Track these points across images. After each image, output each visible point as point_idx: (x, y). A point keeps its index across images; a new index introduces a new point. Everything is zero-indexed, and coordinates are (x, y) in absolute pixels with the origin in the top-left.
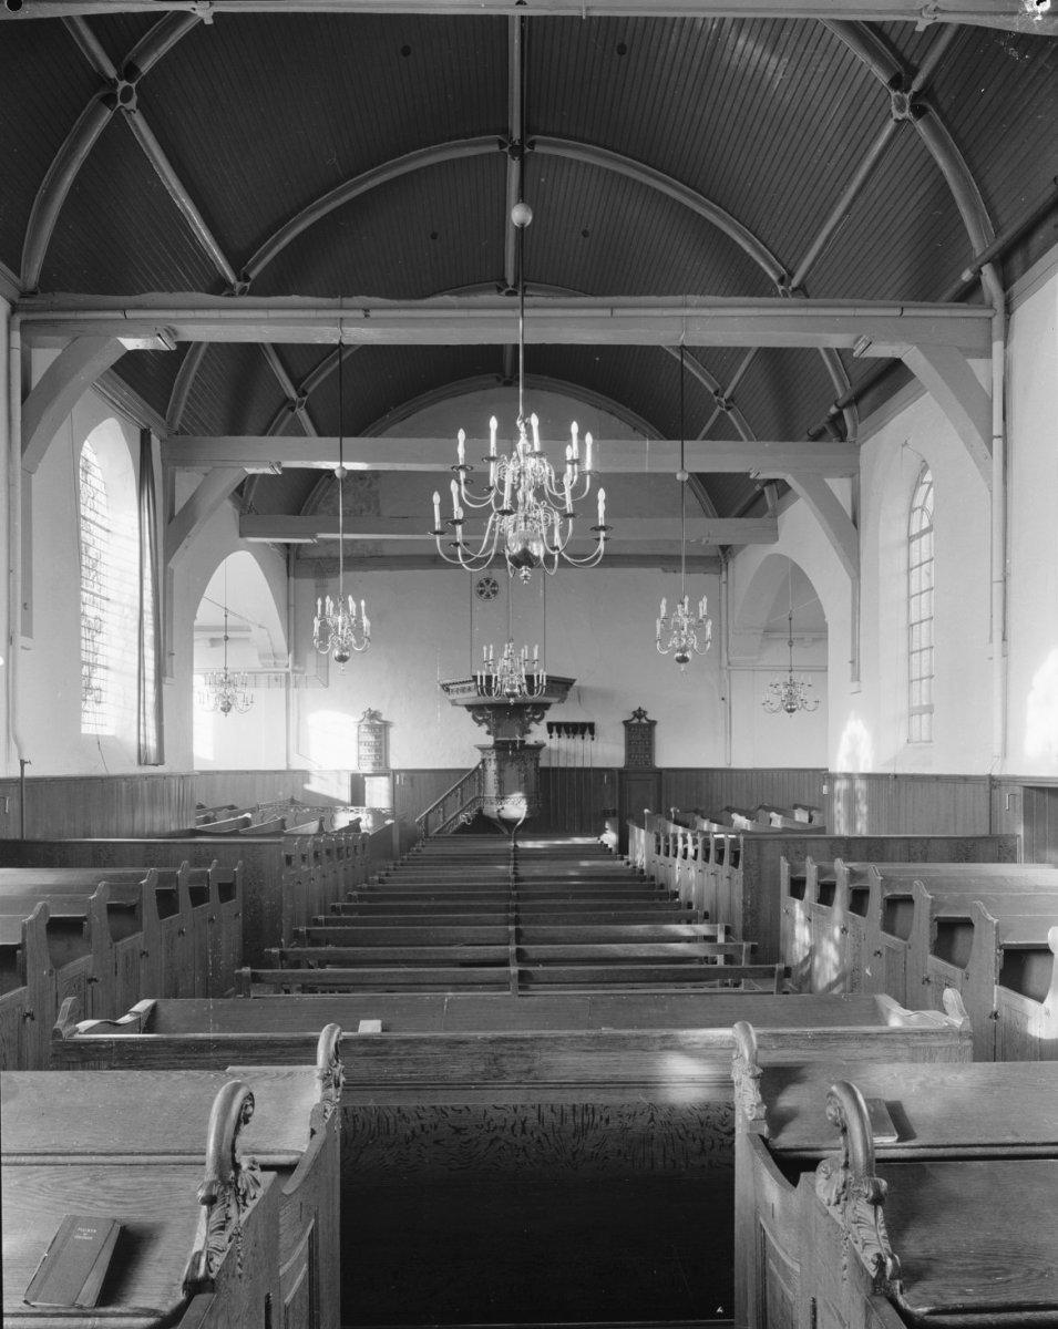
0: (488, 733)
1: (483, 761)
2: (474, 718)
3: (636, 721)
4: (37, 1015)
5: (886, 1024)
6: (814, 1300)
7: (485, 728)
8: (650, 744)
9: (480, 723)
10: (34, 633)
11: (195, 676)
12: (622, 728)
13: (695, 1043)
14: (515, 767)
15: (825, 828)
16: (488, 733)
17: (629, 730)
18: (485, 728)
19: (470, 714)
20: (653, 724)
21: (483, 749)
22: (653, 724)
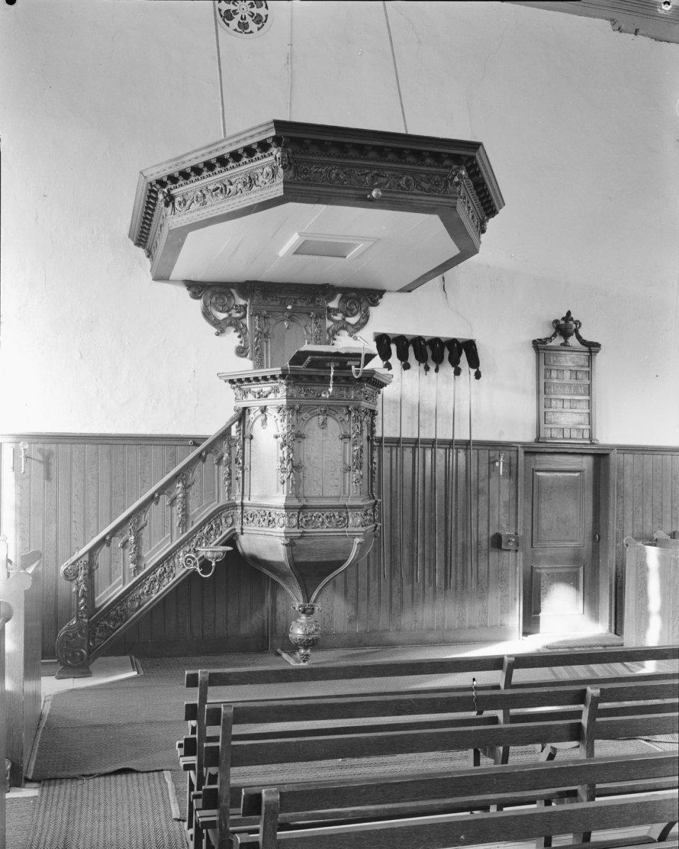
0: (241, 352)
1: (242, 416)
2: (207, 314)
7: (232, 339)
9: (220, 327)
16: (241, 352)
18: (232, 339)
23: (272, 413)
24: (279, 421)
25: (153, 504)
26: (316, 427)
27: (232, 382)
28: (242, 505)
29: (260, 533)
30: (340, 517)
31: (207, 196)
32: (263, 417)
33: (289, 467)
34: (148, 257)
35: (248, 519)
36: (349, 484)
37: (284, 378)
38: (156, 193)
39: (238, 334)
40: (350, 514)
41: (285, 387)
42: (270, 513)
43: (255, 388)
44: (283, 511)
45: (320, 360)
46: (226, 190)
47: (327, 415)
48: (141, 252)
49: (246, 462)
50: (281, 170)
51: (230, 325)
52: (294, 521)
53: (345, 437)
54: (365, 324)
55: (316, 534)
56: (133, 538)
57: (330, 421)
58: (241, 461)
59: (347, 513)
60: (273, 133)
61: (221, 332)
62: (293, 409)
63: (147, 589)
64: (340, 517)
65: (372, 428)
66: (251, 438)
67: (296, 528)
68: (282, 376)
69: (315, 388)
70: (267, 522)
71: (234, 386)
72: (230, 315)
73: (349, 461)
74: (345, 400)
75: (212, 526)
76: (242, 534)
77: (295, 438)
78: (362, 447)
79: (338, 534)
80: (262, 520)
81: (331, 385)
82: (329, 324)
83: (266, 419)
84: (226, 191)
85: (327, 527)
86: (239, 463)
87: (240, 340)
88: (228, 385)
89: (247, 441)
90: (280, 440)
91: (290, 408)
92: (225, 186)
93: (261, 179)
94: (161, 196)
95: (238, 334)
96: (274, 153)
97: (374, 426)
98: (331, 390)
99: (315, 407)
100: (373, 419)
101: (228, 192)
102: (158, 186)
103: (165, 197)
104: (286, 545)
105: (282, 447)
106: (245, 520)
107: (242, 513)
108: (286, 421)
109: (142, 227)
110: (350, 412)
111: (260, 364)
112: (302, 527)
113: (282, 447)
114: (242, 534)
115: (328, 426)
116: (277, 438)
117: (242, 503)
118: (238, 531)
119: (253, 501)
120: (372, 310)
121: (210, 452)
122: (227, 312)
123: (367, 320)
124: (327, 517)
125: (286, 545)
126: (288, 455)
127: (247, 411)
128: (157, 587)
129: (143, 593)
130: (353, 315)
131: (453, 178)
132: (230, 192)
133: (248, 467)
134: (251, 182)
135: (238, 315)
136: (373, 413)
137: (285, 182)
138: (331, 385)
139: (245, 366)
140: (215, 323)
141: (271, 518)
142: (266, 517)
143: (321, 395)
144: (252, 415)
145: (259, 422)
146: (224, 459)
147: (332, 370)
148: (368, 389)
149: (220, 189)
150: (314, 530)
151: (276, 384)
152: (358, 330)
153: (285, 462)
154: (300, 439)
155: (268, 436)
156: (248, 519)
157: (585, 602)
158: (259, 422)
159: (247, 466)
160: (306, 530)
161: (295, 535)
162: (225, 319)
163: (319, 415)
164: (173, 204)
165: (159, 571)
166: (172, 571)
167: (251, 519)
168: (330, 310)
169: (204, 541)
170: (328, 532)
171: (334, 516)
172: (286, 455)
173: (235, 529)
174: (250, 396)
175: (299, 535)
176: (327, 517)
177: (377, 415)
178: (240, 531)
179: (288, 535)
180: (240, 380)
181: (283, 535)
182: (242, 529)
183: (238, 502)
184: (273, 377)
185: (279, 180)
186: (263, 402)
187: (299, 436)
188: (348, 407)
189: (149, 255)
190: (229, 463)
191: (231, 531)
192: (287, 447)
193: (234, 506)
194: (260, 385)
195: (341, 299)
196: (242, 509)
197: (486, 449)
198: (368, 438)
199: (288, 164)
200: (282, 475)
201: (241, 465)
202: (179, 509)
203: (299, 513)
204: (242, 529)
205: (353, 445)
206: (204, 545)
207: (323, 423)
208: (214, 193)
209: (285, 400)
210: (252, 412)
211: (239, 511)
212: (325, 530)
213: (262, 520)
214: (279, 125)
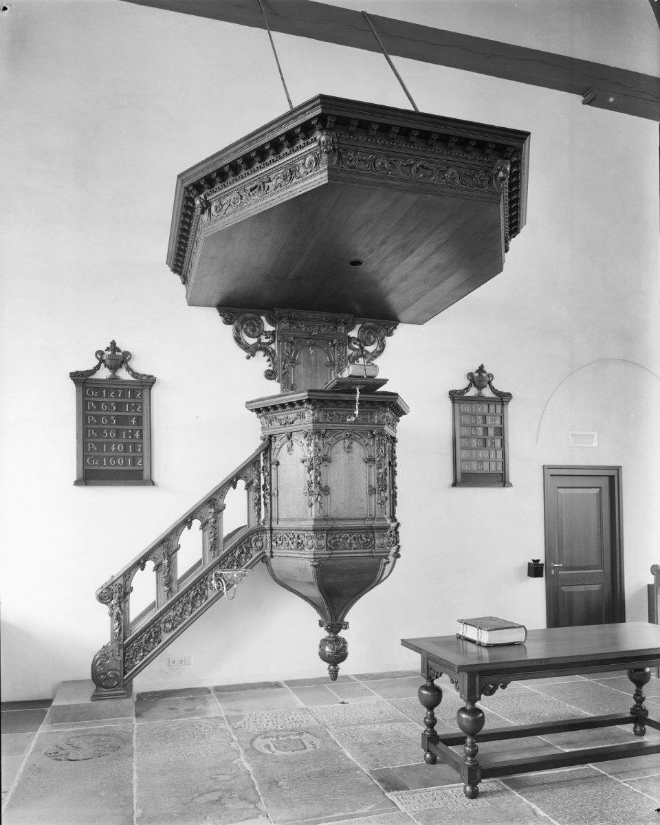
0: (270, 375)
1: (267, 447)
2: (238, 340)
3: (104, 373)
4: (335, 332)
5: (543, 564)
6: (537, 442)
7: (261, 363)
8: (139, 420)
9: (251, 351)
10: (527, 130)
11: (530, 657)
12: (70, 392)
13: (383, 243)
14: (359, 451)
15: (460, 426)
16: (270, 375)
17: (84, 388)
18: (261, 363)
19: (230, 329)
20: (148, 383)
21: (263, 410)
22: (148, 383)
23: (299, 440)
24: (305, 447)
25: (186, 528)
26: (342, 451)
27: (258, 411)
28: (271, 529)
29: (289, 555)
30: (367, 538)
31: (244, 198)
32: (289, 443)
33: (316, 491)
34: (184, 283)
35: (277, 543)
36: (375, 506)
37: (310, 404)
38: (193, 201)
39: (267, 358)
40: (376, 535)
41: (311, 412)
42: (298, 536)
43: (281, 415)
44: (312, 534)
45: (345, 387)
46: (264, 187)
47: (352, 439)
48: (177, 278)
49: (273, 488)
50: (325, 158)
51: (260, 349)
52: (323, 543)
53: (370, 460)
54: (381, 352)
55: (344, 555)
56: (166, 561)
57: (355, 445)
58: (268, 487)
59: (373, 534)
60: (318, 111)
61: (251, 355)
62: (318, 433)
63: (180, 611)
64: (367, 538)
65: (392, 455)
66: (278, 464)
67: (325, 549)
68: (309, 401)
69: (340, 413)
70: (295, 544)
71: (261, 415)
72: (259, 341)
73: (374, 483)
74: (369, 424)
75: (243, 549)
76: (272, 557)
77: (321, 461)
78: (386, 470)
79: (366, 555)
80: (290, 542)
81: (357, 407)
82: (350, 352)
83: (292, 444)
84: (264, 189)
85: (355, 548)
86: (267, 489)
87: (269, 363)
88: (254, 414)
89: (274, 466)
90: (307, 463)
91: (317, 432)
92: (263, 183)
93: (302, 170)
94: (198, 202)
95: (267, 358)
96: (318, 137)
97: (395, 453)
98: (357, 412)
99: (340, 431)
100: (393, 445)
101: (266, 189)
102: (195, 192)
103: (201, 203)
104: (315, 566)
105: (309, 470)
106: (274, 544)
107: (271, 537)
108: (312, 445)
109: (175, 265)
110: (374, 436)
111: (289, 386)
112: (331, 549)
113: (309, 470)
114: (272, 557)
115: (354, 449)
116: (303, 462)
117: (271, 526)
118: (268, 554)
119: (281, 525)
120: (387, 339)
121: (240, 478)
122: (257, 337)
123: (384, 349)
124: (355, 538)
125: (315, 566)
126: (316, 478)
127: (273, 438)
128: (190, 609)
129: (177, 614)
130: (372, 343)
131: (498, 173)
132: (268, 188)
133: (276, 492)
134: (292, 173)
135: (267, 340)
136: (393, 440)
137: (330, 169)
138: (357, 407)
139: (273, 389)
140: (246, 347)
141: (300, 541)
142: (295, 540)
143: (346, 420)
144: (277, 442)
145: (285, 448)
146: (254, 485)
147: (358, 393)
148: (389, 414)
149: (258, 187)
150: (342, 551)
151: (303, 410)
152: (376, 357)
153: (313, 485)
154: (326, 463)
155: (293, 464)
156: (277, 543)
157: (174, 548)
158: (285, 448)
159: (274, 491)
160: (334, 551)
161: (325, 556)
162: (255, 344)
163: (344, 439)
164: (210, 210)
165: (192, 594)
166: (204, 593)
167: (279, 542)
168: (350, 339)
169: (235, 564)
170: (356, 553)
171: (361, 537)
172: (313, 477)
173: (265, 552)
174: (276, 424)
175: (328, 556)
176: (355, 538)
177: (397, 442)
178: (270, 554)
179: (316, 556)
180: (267, 409)
181: (312, 556)
182: (272, 552)
183: (267, 526)
184: (300, 403)
185: (323, 167)
186: (289, 429)
187: (326, 460)
188: (372, 432)
189: (185, 281)
190: (258, 490)
191: (262, 553)
192: (314, 470)
193: (264, 531)
194: (286, 412)
195: (360, 329)
196: (271, 533)
197: (285, 520)
198: (390, 463)
199: (336, 152)
200: (310, 497)
201: (269, 491)
202: (211, 533)
203: (327, 534)
204: (272, 552)
205: (378, 468)
206: (235, 567)
207: (349, 447)
208: (251, 193)
209: (312, 425)
210: (278, 439)
211: (268, 535)
212: (352, 551)
213: (290, 542)
214: (324, 100)
